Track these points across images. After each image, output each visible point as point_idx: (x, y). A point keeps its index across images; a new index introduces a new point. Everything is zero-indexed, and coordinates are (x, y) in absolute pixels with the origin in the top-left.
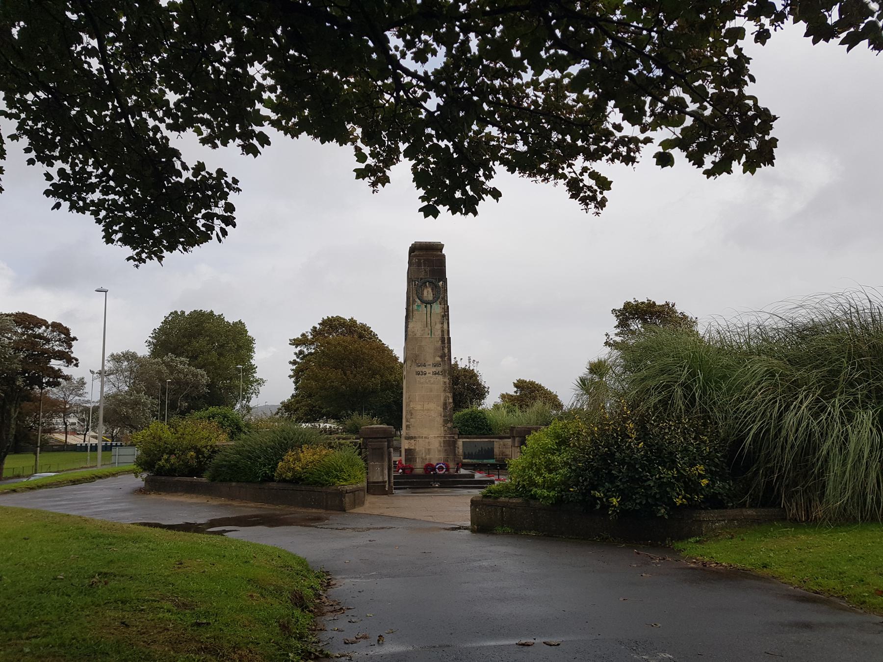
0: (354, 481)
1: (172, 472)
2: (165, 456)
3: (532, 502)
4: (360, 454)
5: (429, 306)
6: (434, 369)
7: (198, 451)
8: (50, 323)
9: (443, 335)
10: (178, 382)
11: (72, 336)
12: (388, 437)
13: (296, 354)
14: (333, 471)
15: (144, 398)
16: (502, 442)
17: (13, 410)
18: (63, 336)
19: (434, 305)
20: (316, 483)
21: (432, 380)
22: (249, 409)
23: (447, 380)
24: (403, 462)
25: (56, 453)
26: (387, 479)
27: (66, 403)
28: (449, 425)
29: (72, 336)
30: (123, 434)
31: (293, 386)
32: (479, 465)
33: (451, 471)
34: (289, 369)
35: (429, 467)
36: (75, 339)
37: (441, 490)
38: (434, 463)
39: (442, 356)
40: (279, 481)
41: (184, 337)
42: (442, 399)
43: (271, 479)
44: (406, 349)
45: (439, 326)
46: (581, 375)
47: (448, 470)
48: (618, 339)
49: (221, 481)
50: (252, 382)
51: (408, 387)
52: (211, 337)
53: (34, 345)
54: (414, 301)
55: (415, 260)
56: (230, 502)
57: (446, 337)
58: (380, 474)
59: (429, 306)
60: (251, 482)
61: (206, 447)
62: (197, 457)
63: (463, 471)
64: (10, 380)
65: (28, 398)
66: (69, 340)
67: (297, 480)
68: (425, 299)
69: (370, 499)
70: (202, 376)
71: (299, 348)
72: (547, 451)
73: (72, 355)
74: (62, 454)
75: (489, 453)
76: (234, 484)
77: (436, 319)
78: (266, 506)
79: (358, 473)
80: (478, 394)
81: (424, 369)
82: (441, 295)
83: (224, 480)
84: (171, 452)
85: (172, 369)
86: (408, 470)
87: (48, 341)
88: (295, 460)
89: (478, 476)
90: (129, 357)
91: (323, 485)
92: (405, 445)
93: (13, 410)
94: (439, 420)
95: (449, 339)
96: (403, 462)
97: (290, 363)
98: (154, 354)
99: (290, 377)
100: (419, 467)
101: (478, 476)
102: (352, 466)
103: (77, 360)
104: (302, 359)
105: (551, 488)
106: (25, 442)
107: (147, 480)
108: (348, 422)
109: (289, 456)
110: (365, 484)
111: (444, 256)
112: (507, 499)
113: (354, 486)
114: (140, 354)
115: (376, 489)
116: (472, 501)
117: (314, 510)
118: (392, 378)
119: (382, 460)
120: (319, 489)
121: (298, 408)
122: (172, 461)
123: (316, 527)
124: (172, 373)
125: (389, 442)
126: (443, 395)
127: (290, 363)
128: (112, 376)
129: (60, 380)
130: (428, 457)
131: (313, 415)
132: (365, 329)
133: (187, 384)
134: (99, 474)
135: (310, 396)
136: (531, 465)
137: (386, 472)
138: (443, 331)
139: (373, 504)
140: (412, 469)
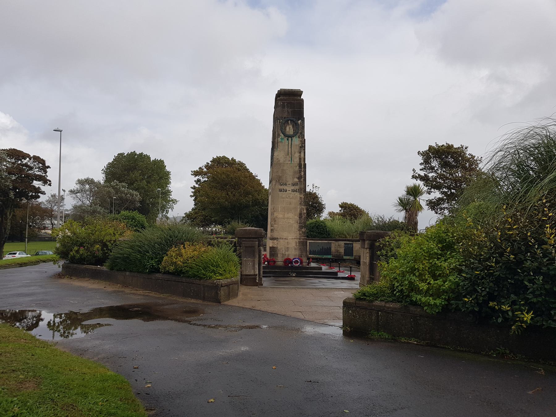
0: (228, 276)
1: (82, 261)
2: (76, 248)
3: (412, 308)
4: (234, 251)
5: (290, 139)
6: (293, 188)
7: (104, 245)
8: (32, 156)
9: (300, 161)
10: (121, 199)
11: (46, 165)
12: (260, 238)
13: (195, 181)
14: (210, 267)
15: (99, 209)
16: (337, 243)
17: (8, 213)
18: (41, 165)
19: (294, 139)
20: (195, 276)
21: (291, 196)
22: (167, 218)
23: (302, 196)
24: (268, 256)
25: (46, 242)
26: (257, 273)
27: (52, 211)
28: (303, 230)
29: (46, 165)
30: (543, 249)
31: (193, 203)
32: (320, 259)
33: (304, 264)
34: (190, 192)
35: (288, 261)
36: (48, 167)
37: (296, 279)
38: (292, 258)
39: (300, 178)
40: (164, 273)
41: (125, 170)
42: (299, 210)
43: (157, 271)
44: (272, 173)
45: (297, 155)
46: (400, 196)
47: (301, 263)
48: (422, 173)
49: (118, 270)
50: (169, 201)
51: (272, 201)
52: (142, 171)
53: (21, 171)
54: (279, 135)
55: (280, 103)
56: (123, 289)
57: (303, 163)
58: (251, 268)
59: (290, 139)
60: (140, 272)
61: (110, 241)
62: (102, 249)
63: (313, 265)
64: (6, 194)
65: (18, 206)
66: (45, 168)
67: (178, 273)
68: (287, 133)
69: (243, 290)
70: (136, 195)
71: (197, 177)
72: (431, 255)
73: (48, 178)
74: (50, 242)
75: (328, 251)
76: (128, 273)
77: (296, 149)
78: (153, 294)
79: (233, 268)
80: (318, 210)
81: (285, 187)
82: (299, 131)
83: (119, 270)
84: (81, 245)
85: (117, 191)
86: (271, 263)
87: (31, 168)
88: (177, 255)
89: (325, 268)
90: (89, 181)
91: (201, 278)
92: (270, 244)
93: (8, 213)
94: (296, 226)
95: (305, 165)
96: (268, 256)
97: (192, 188)
98: (107, 180)
99: (191, 196)
100: (280, 260)
101: (325, 268)
102: (228, 262)
103: (50, 181)
104: (199, 185)
105: (437, 294)
106: (18, 236)
107: (64, 267)
108: (229, 227)
109: (173, 252)
110: (239, 278)
111: (302, 100)
112: (383, 304)
113: (229, 280)
114: (96, 180)
115: (249, 281)
116: (345, 303)
117: (193, 301)
118: (259, 197)
119: (254, 256)
120: (198, 281)
121: (196, 217)
122: (81, 252)
123: (189, 322)
124: (117, 193)
125: (259, 241)
126: (299, 207)
127: (192, 188)
128: (78, 194)
129: (39, 194)
130: (287, 253)
131: (206, 222)
132: (241, 165)
133: (127, 200)
134: (44, 259)
135: (204, 209)
136: (413, 270)
137: (257, 266)
138: (300, 159)
139: (246, 297)
140: (275, 262)
